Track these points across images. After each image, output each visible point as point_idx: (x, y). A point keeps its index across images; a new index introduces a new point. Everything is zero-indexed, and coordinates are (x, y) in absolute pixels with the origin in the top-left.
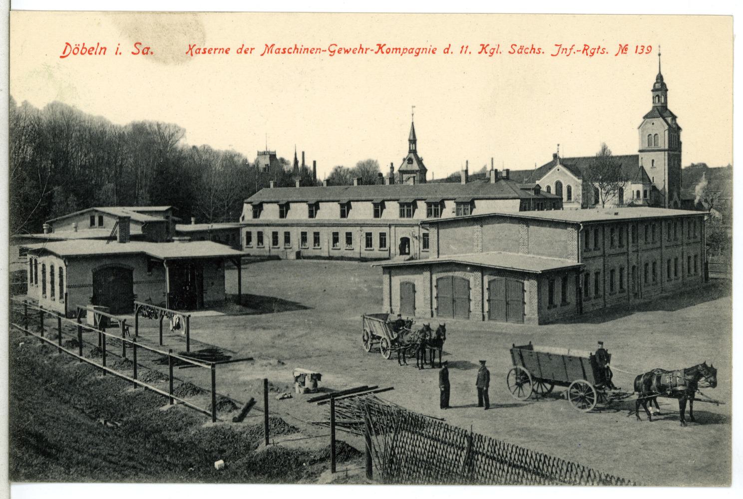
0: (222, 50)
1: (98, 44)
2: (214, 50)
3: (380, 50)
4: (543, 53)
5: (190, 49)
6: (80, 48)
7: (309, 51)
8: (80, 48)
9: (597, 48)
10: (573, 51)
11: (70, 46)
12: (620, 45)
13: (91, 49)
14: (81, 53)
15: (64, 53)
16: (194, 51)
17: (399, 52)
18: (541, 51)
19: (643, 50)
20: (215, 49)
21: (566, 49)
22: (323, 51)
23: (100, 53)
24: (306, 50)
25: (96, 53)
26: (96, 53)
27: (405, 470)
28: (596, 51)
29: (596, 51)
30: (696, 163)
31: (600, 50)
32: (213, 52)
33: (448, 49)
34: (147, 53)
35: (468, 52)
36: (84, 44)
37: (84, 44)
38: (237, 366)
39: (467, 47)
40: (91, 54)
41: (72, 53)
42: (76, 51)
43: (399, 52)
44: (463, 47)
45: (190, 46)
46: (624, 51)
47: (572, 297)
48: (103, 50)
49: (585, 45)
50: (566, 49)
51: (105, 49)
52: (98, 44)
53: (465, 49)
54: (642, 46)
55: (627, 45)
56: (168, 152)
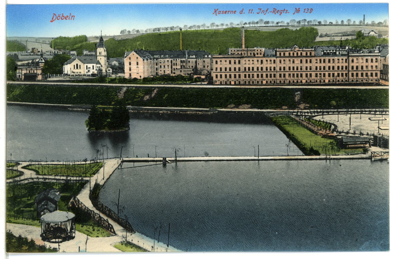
0: (232, 12)
1: (70, 14)
2: (227, 12)
3: (215, 13)
4: (289, 13)
5: (215, 11)
6: (61, 16)
7: (233, 12)
8: (61, 16)
9: (283, 10)
10: (267, 12)
11: (55, 15)
12: (296, 9)
13: (67, 17)
14: (62, 19)
15: (53, 19)
16: (217, 12)
17: (264, 13)
18: (288, 12)
19: (308, 11)
20: (228, 11)
21: (264, 11)
22: (271, 12)
23: (251, 13)
24: (232, 12)
25: (69, 19)
26: (69, 19)
27: (220, 227)
28: (283, 12)
29: (283, 12)
30: (80, 35)
31: (285, 11)
32: (227, 13)
33: (242, 11)
34: (220, 13)
35: (252, 13)
36: (63, 14)
37: (63, 14)
38: (106, 150)
39: (252, 10)
40: (67, 19)
41: (56, 19)
42: (63, 18)
43: (264, 13)
44: (250, 10)
45: (215, 10)
46: (298, 12)
47: (386, 157)
48: (73, 17)
49: (274, 9)
50: (264, 11)
51: (74, 16)
52: (70, 14)
53: (251, 11)
54: (308, 9)
55: (299, 8)
56: (186, 82)
